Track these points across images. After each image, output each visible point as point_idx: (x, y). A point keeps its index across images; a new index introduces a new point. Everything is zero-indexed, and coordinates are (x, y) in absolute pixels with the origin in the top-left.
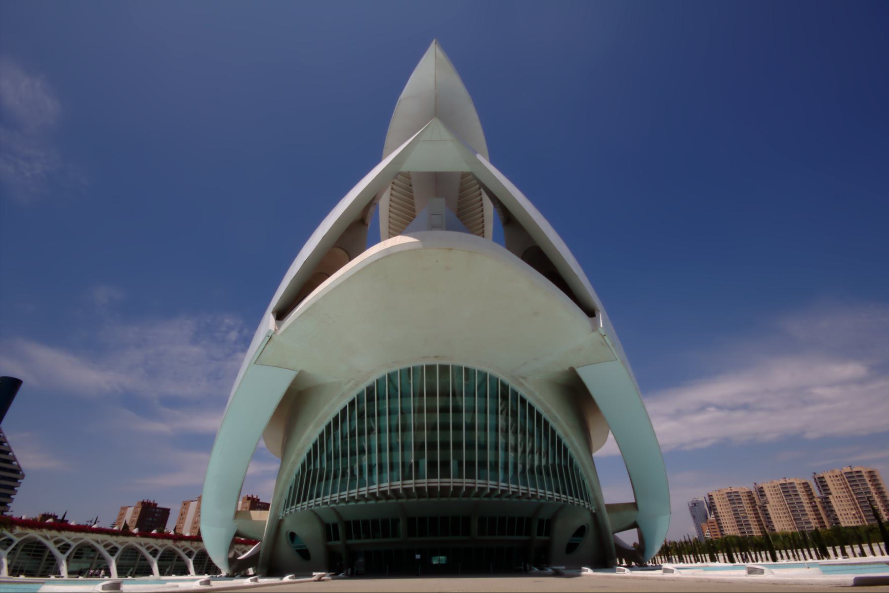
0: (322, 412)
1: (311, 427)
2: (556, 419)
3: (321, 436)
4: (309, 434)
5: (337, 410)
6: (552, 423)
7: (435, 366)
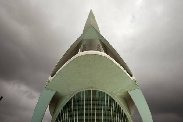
0: (61, 104)
1: (59, 108)
2: (123, 107)
3: (67, 103)
4: (59, 110)
5: (66, 103)
6: (120, 106)
7: (91, 90)
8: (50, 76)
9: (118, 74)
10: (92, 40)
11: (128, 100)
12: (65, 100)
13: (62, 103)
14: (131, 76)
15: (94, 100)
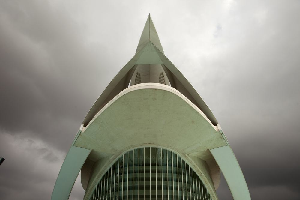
0: (101, 170)
1: (96, 177)
2: (201, 175)
4: (97, 180)
5: (107, 169)
6: (200, 177)
7: (149, 148)
8: (82, 125)
9: (193, 122)
10: (150, 66)
11: (210, 165)
12: (106, 164)
13: (102, 169)
14: (215, 124)
15: (153, 165)
